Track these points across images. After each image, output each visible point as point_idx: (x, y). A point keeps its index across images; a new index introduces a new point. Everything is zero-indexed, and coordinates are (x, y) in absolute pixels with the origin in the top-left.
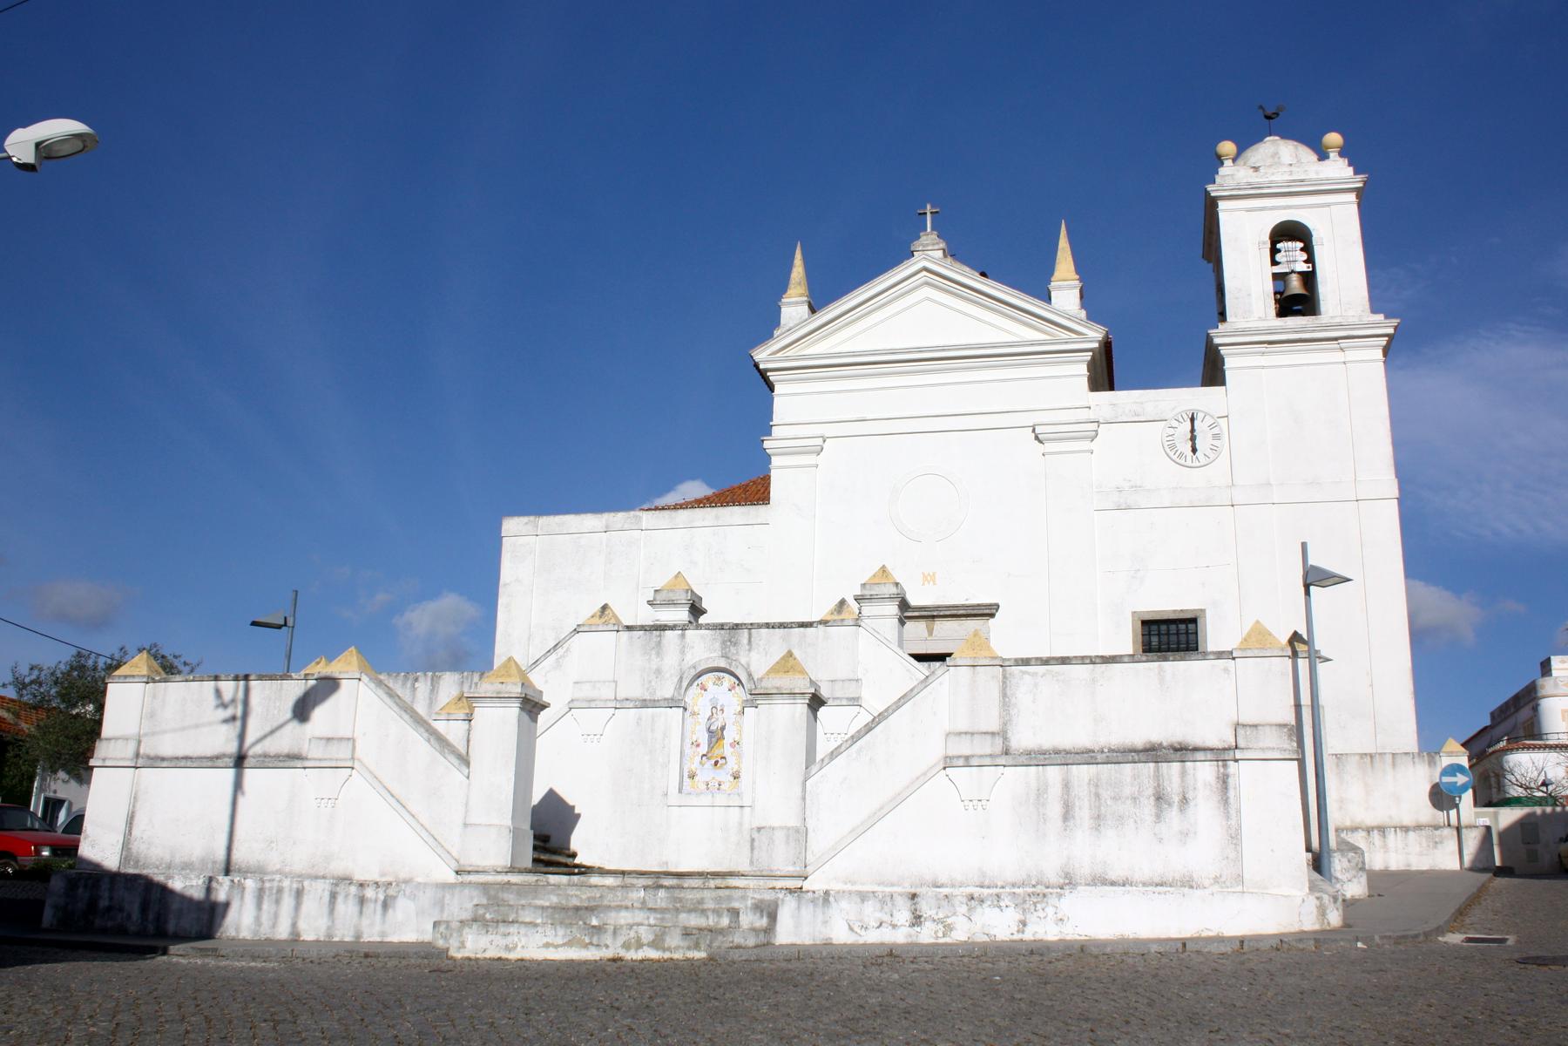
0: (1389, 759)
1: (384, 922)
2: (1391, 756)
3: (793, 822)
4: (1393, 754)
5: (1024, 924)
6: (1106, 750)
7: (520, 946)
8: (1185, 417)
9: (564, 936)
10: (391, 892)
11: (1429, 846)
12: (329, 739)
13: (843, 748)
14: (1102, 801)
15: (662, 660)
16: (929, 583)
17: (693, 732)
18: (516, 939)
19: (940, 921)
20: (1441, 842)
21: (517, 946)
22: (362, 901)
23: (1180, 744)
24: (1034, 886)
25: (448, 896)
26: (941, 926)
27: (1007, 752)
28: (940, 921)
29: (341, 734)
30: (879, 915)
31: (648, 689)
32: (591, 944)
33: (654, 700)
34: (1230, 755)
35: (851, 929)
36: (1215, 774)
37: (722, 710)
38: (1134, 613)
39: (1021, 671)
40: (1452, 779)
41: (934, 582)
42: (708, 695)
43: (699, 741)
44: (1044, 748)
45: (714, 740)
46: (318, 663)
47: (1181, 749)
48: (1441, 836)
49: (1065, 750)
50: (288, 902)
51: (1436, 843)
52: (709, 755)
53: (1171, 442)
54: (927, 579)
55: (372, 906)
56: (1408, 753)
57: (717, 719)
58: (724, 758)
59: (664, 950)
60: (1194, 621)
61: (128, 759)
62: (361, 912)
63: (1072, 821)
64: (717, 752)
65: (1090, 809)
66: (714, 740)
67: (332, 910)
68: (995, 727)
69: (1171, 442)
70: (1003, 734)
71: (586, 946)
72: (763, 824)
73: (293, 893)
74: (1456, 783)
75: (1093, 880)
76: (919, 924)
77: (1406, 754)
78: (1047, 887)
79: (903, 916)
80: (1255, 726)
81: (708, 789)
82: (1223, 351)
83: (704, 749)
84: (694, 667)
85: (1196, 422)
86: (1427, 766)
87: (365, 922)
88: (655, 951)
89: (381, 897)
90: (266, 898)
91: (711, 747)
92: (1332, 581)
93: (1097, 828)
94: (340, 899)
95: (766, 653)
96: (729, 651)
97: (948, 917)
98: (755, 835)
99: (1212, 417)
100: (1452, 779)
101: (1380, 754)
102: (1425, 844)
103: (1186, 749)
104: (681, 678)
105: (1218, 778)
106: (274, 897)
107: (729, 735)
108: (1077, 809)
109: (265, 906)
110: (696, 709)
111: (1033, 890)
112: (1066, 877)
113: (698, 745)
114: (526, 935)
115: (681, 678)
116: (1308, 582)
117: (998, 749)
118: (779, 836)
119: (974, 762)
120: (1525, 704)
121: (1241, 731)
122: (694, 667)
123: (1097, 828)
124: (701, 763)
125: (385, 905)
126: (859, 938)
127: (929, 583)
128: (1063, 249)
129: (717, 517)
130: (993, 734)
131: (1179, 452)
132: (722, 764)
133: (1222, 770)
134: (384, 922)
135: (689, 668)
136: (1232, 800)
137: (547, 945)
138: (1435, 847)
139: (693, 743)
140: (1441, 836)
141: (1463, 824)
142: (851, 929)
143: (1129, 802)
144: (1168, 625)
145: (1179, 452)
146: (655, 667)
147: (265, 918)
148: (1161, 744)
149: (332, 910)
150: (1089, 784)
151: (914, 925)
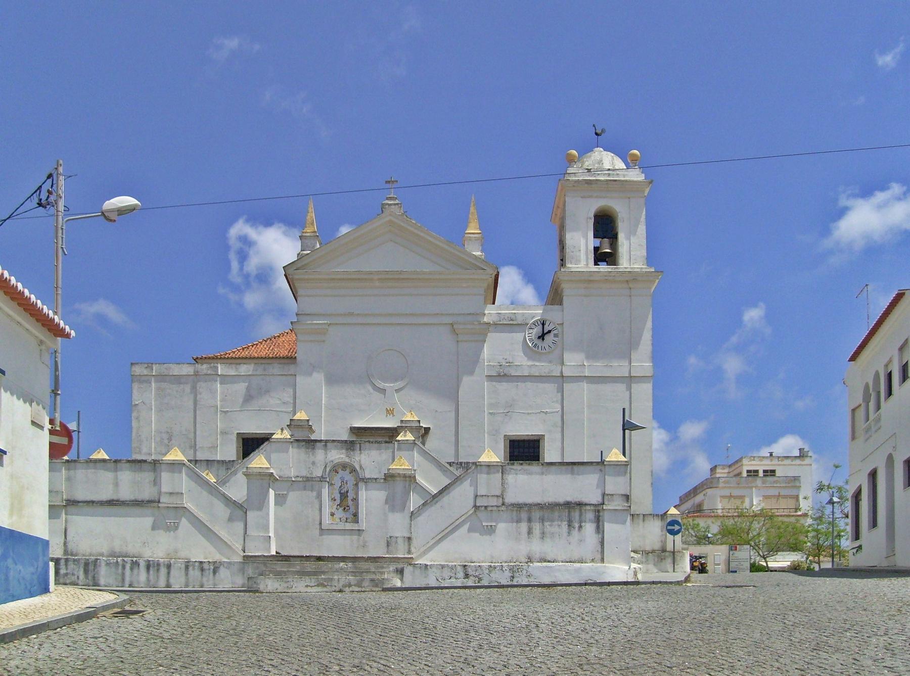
0: (641, 517)
1: (214, 579)
2: (642, 516)
3: (407, 535)
4: (644, 515)
5: (513, 577)
6: (547, 504)
7: (294, 586)
8: (539, 323)
9: (314, 582)
10: (216, 565)
11: (658, 560)
12: (171, 493)
13: (429, 502)
14: (545, 527)
15: (315, 457)
16: (390, 415)
17: (332, 494)
18: (292, 584)
19: (476, 576)
20: (665, 559)
21: (292, 587)
22: (202, 570)
23: (579, 502)
24: (515, 562)
25: (246, 567)
26: (477, 578)
27: (503, 504)
28: (476, 576)
29: (177, 491)
30: (450, 574)
31: (308, 471)
32: (328, 585)
33: (313, 478)
34: (600, 508)
35: (438, 580)
36: (594, 515)
37: (347, 483)
38: (505, 436)
39: (510, 468)
40: (673, 528)
41: (393, 414)
42: (339, 476)
43: (336, 498)
44: (520, 503)
45: (343, 498)
46: (99, 452)
47: (579, 504)
48: (664, 556)
49: (529, 504)
50: (163, 571)
51: (662, 559)
52: (341, 505)
53: (530, 337)
54: (389, 412)
55: (207, 571)
56: (651, 514)
57: (344, 488)
58: (349, 506)
59: (362, 587)
60: (538, 441)
61: (319, 496)
62: (202, 575)
63: (532, 535)
64: (344, 503)
65: (540, 530)
66: (343, 498)
67: (187, 574)
68: (498, 493)
69: (530, 337)
70: (502, 496)
71: (325, 586)
72: (393, 535)
73: (166, 566)
74: (674, 529)
75: (540, 560)
76: (468, 578)
77: (650, 514)
78: (521, 563)
79: (461, 574)
80: (612, 495)
81: (341, 521)
82: (563, 285)
83: (338, 501)
84: (332, 462)
85: (545, 326)
86: (660, 521)
87: (205, 579)
88: (357, 588)
89: (212, 567)
90: (151, 568)
91: (342, 500)
92: (636, 428)
93: (542, 538)
94: (191, 568)
95: (369, 455)
96: (350, 454)
97: (480, 574)
98: (389, 539)
99: (554, 324)
100: (673, 528)
101: (637, 514)
102: (656, 560)
103: (582, 504)
104: (326, 466)
105: (595, 517)
106: (156, 568)
107: (351, 495)
108: (534, 530)
109: (151, 572)
110: (333, 482)
111: (515, 564)
112: (529, 559)
113: (335, 500)
114: (297, 582)
115: (326, 466)
116: (625, 428)
117: (500, 503)
118: (400, 541)
119: (489, 509)
120: (700, 492)
121: (606, 497)
122: (332, 462)
123: (542, 538)
124: (337, 509)
125: (215, 572)
126: (440, 583)
127: (390, 415)
128: (472, 213)
129: (265, 370)
130: (497, 496)
131: (534, 344)
132: (348, 509)
133: (597, 514)
134: (214, 579)
135: (330, 462)
136: (601, 527)
137: (307, 586)
138: (661, 561)
139: (332, 499)
140: (664, 556)
141: (675, 551)
142: (438, 580)
143: (557, 527)
144: (293, 403)
145: (534, 344)
146: (311, 461)
147: (151, 577)
148: (571, 502)
149: (187, 574)
150: (539, 519)
151: (465, 578)
